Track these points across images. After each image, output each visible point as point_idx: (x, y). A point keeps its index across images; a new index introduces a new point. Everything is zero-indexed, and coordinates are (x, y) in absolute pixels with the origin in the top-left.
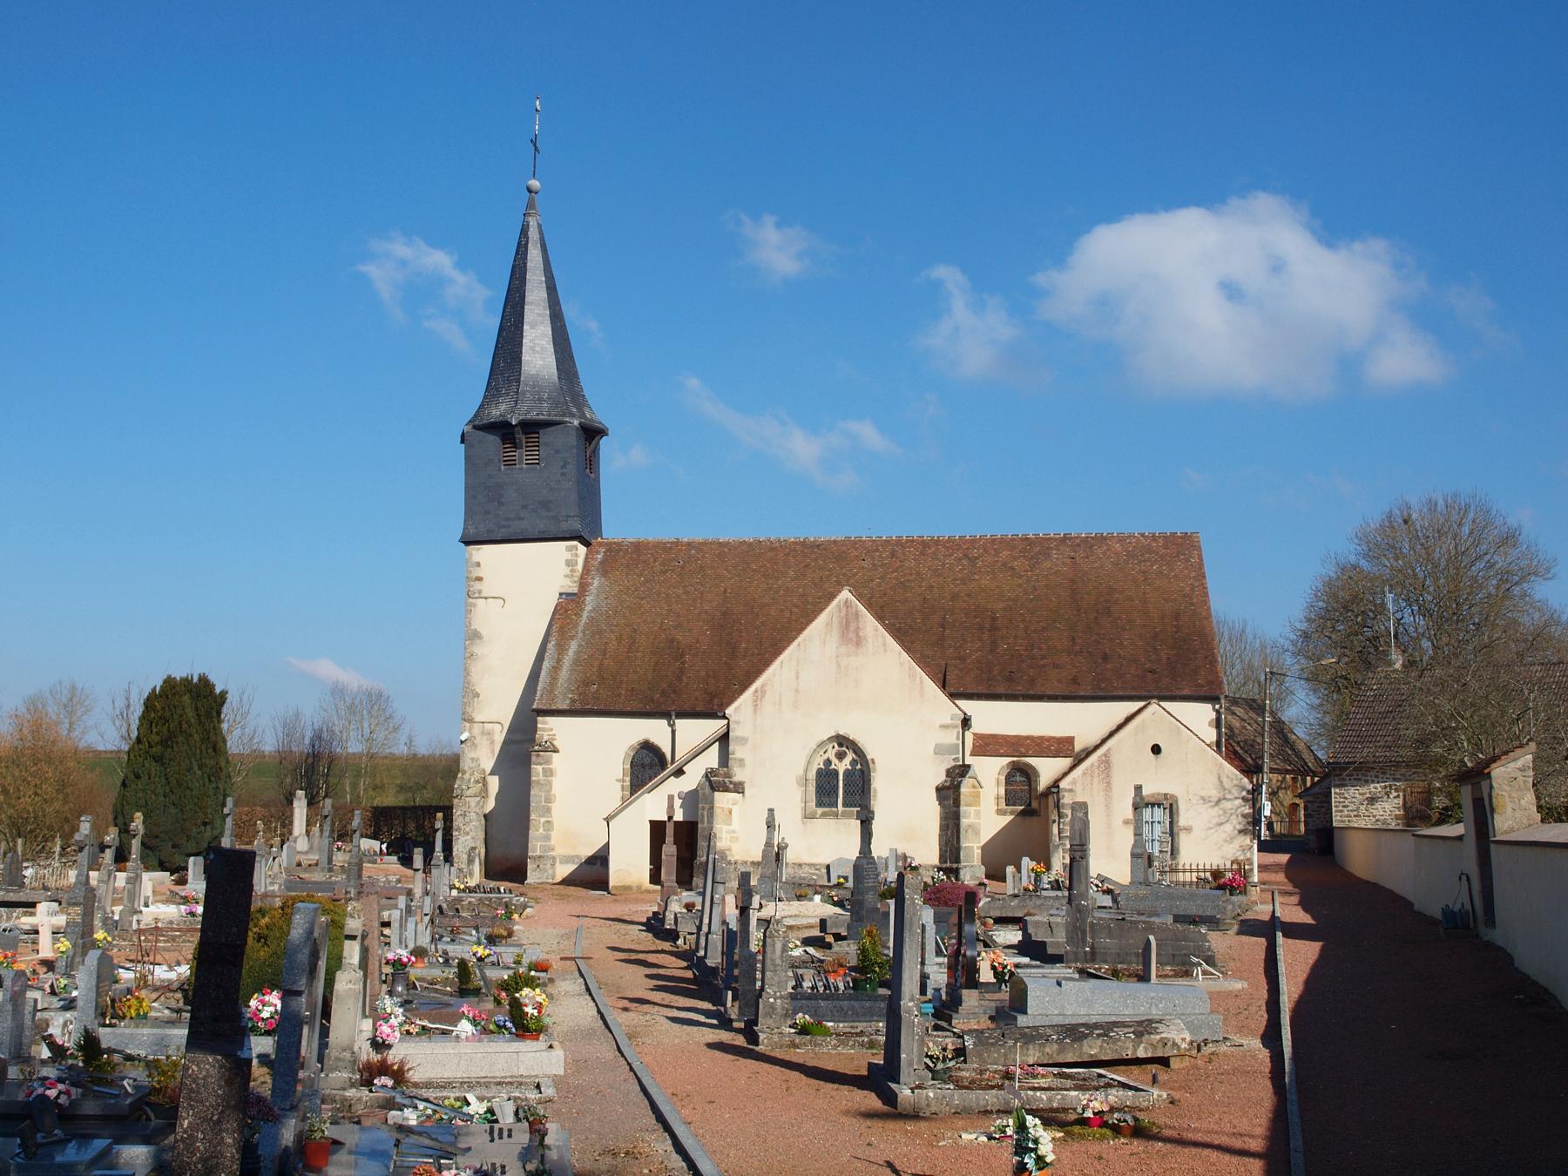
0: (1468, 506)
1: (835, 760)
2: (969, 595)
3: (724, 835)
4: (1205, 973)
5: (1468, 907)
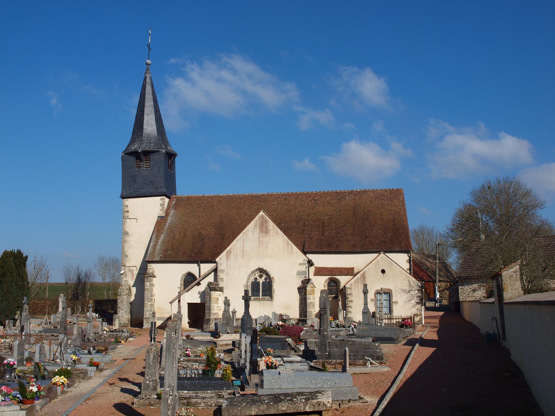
0: (512, 182)
1: (258, 278)
2: (314, 214)
3: (215, 308)
4: (371, 364)
5: (496, 332)
